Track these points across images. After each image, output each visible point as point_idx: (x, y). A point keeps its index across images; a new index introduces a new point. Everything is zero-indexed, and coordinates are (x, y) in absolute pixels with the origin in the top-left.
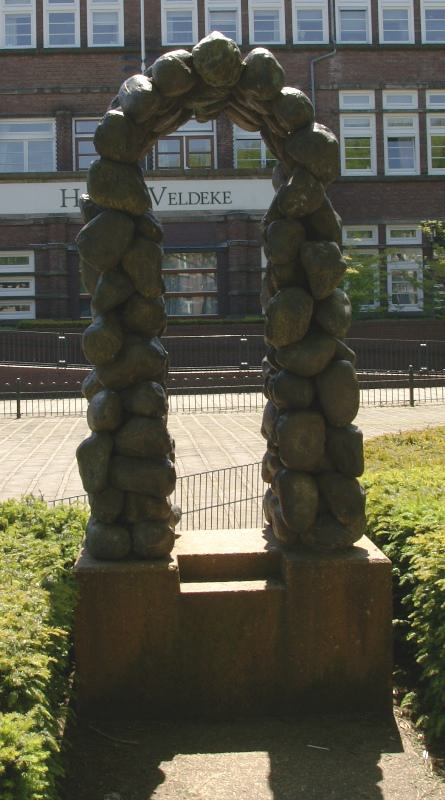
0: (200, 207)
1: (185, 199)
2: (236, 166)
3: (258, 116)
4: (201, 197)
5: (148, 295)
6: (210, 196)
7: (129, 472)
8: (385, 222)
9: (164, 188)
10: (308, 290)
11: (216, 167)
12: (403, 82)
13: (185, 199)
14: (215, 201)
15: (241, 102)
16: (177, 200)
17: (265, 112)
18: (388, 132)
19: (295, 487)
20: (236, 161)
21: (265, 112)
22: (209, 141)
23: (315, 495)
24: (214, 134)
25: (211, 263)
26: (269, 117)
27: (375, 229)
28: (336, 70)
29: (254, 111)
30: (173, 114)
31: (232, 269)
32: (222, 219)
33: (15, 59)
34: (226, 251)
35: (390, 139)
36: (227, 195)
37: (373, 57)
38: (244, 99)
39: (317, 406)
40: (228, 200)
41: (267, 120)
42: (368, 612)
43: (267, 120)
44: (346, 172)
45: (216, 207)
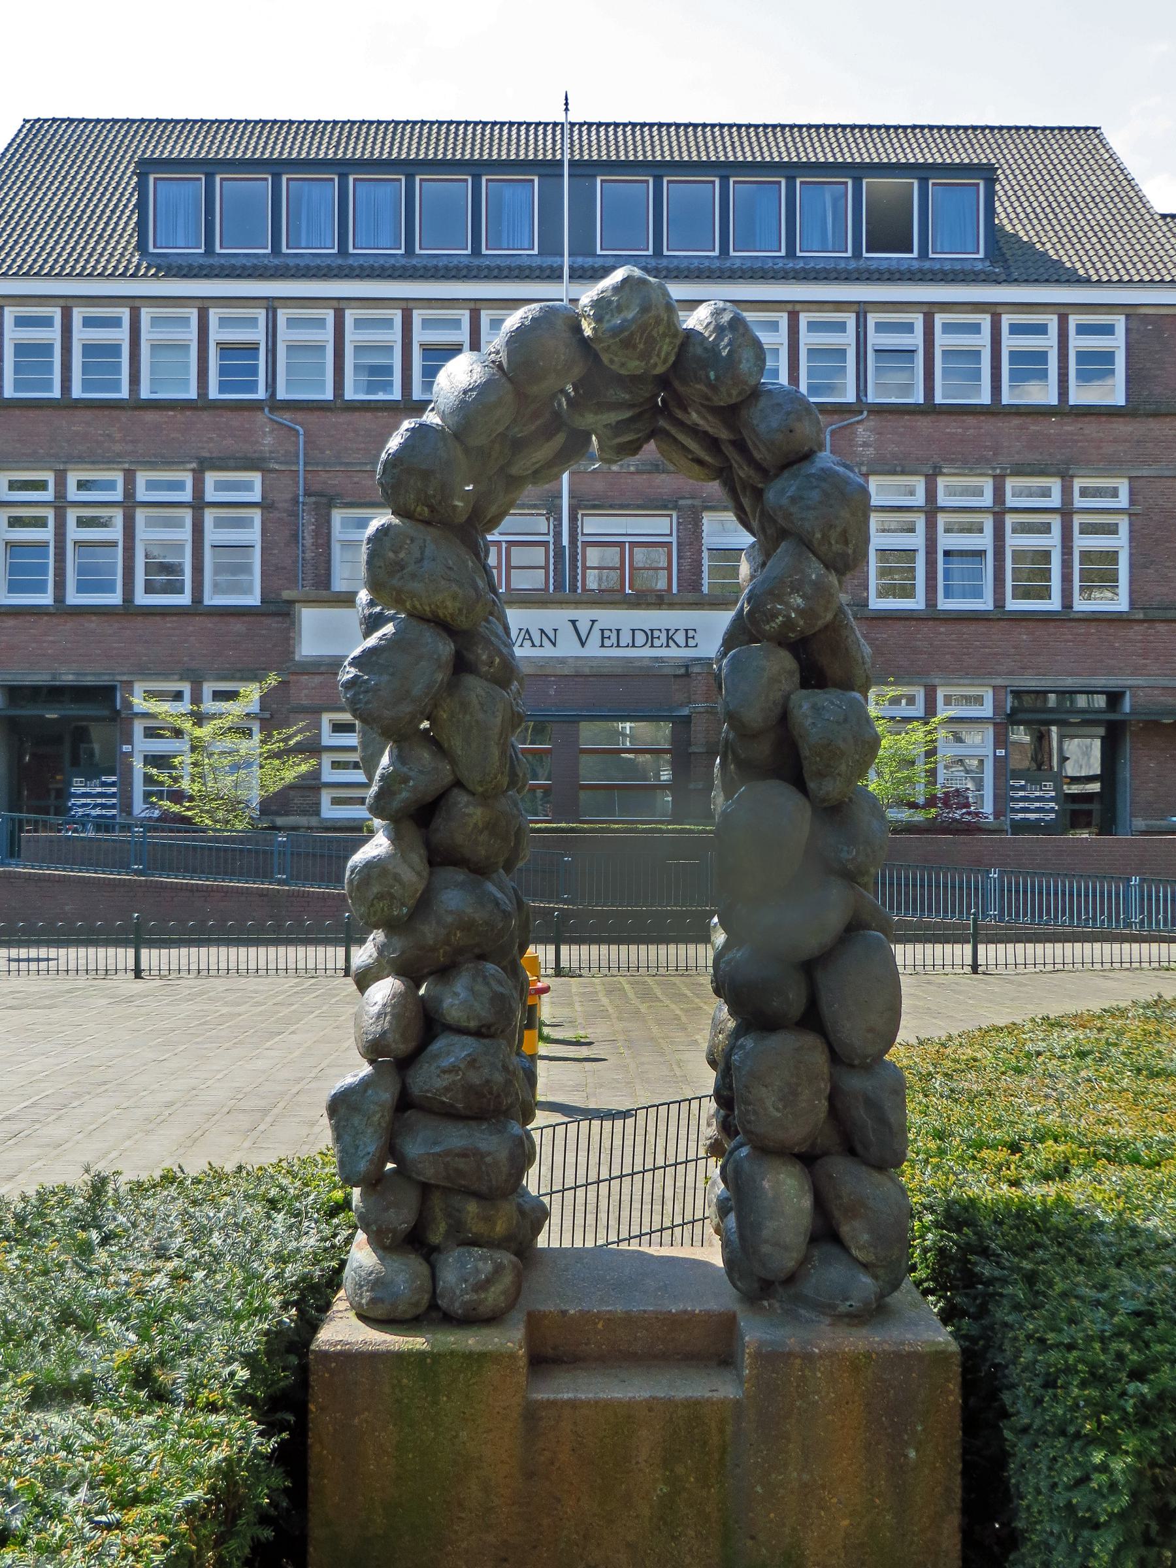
0: (648, 652)
1: (626, 639)
2: (705, 589)
3: (713, 444)
4: (650, 636)
5: (480, 789)
6: (663, 636)
7: (437, 1132)
8: (936, 681)
9: (593, 621)
10: (799, 783)
11: (675, 591)
12: (970, 463)
13: (626, 639)
14: (671, 643)
15: (679, 414)
16: (614, 640)
17: (724, 435)
18: (945, 541)
19: (766, 1184)
20: (706, 581)
21: (724, 435)
22: (662, 551)
23: (807, 1203)
24: (673, 539)
25: (666, 728)
26: (733, 443)
27: (920, 693)
28: (865, 445)
29: (706, 433)
30: (548, 439)
31: (693, 749)
32: (682, 671)
33: (369, 415)
34: (687, 720)
35: (947, 553)
36: (691, 634)
37: (924, 424)
38: (685, 409)
39: (812, 1019)
40: (691, 642)
41: (729, 451)
42: (912, 1454)
43: (729, 451)
44: (877, 603)
45: (673, 652)
